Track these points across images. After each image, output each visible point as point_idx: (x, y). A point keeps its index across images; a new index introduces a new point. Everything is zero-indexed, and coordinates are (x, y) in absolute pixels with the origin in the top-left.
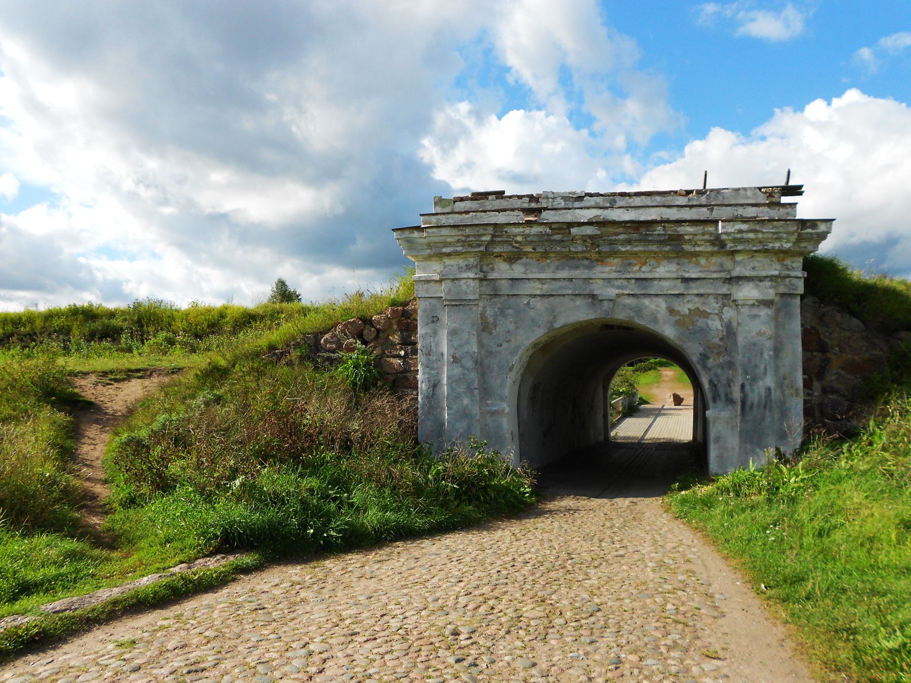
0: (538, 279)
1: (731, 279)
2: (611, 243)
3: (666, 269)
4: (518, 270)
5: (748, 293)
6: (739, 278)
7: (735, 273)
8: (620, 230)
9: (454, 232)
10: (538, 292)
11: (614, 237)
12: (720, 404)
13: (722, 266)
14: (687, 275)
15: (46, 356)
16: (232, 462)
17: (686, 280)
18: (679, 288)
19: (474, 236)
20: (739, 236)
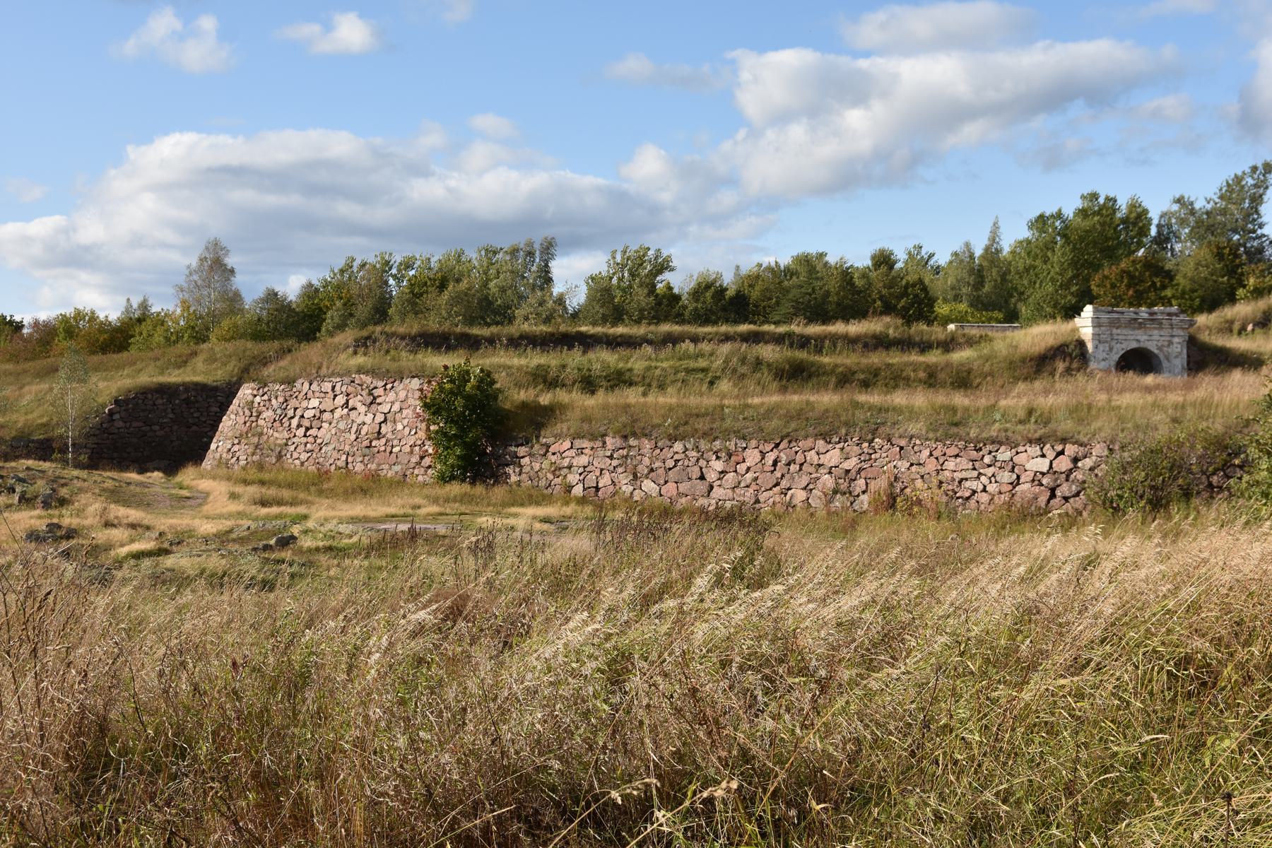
3: (1156, 332)
5: (1176, 340)
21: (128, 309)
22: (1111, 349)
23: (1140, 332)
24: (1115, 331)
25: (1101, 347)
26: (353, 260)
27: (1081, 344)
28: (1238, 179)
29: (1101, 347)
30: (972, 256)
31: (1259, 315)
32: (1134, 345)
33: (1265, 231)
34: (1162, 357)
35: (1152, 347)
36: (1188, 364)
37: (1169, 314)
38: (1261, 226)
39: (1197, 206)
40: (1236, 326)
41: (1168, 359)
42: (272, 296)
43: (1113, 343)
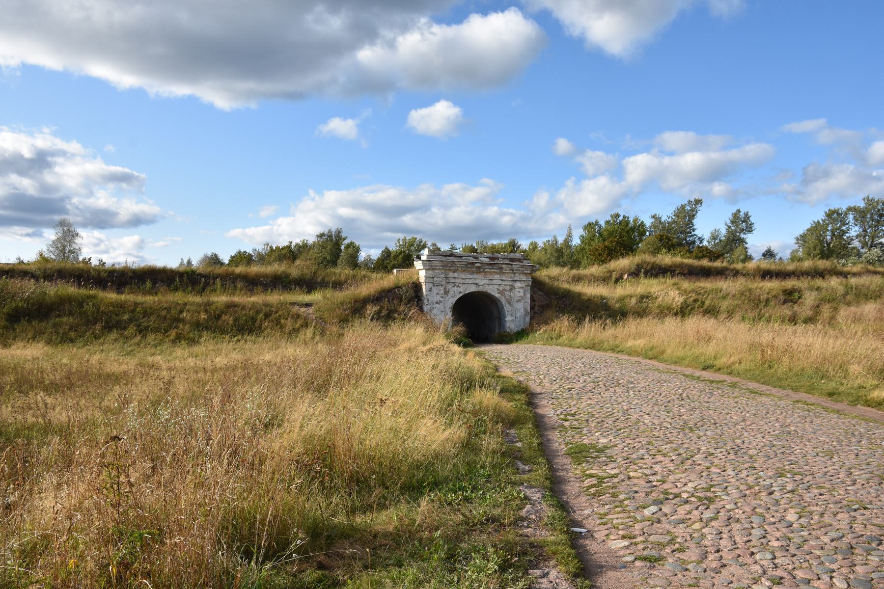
3: (497, 277)
4: (456, 275)
5: (518, 284)
18: (500, 282)
21: (182, 264)
22: (446, 292)
23: (479, 276)
24: (451, 275)
25: (435, 290)
27: (417, 286)
28: (683, 207)
29: (435, 290)
30: (557, 242)
31: (633, 268)
32: (473, 289)
33: (696, 232)
34: (503, 301)
35: (493, 291)
36: (532, 308)
37: (512, 260)
38: (694, 230)
39: (663, 220)
40: (614, 276)
41: (510, 303)
43: (449, 286)
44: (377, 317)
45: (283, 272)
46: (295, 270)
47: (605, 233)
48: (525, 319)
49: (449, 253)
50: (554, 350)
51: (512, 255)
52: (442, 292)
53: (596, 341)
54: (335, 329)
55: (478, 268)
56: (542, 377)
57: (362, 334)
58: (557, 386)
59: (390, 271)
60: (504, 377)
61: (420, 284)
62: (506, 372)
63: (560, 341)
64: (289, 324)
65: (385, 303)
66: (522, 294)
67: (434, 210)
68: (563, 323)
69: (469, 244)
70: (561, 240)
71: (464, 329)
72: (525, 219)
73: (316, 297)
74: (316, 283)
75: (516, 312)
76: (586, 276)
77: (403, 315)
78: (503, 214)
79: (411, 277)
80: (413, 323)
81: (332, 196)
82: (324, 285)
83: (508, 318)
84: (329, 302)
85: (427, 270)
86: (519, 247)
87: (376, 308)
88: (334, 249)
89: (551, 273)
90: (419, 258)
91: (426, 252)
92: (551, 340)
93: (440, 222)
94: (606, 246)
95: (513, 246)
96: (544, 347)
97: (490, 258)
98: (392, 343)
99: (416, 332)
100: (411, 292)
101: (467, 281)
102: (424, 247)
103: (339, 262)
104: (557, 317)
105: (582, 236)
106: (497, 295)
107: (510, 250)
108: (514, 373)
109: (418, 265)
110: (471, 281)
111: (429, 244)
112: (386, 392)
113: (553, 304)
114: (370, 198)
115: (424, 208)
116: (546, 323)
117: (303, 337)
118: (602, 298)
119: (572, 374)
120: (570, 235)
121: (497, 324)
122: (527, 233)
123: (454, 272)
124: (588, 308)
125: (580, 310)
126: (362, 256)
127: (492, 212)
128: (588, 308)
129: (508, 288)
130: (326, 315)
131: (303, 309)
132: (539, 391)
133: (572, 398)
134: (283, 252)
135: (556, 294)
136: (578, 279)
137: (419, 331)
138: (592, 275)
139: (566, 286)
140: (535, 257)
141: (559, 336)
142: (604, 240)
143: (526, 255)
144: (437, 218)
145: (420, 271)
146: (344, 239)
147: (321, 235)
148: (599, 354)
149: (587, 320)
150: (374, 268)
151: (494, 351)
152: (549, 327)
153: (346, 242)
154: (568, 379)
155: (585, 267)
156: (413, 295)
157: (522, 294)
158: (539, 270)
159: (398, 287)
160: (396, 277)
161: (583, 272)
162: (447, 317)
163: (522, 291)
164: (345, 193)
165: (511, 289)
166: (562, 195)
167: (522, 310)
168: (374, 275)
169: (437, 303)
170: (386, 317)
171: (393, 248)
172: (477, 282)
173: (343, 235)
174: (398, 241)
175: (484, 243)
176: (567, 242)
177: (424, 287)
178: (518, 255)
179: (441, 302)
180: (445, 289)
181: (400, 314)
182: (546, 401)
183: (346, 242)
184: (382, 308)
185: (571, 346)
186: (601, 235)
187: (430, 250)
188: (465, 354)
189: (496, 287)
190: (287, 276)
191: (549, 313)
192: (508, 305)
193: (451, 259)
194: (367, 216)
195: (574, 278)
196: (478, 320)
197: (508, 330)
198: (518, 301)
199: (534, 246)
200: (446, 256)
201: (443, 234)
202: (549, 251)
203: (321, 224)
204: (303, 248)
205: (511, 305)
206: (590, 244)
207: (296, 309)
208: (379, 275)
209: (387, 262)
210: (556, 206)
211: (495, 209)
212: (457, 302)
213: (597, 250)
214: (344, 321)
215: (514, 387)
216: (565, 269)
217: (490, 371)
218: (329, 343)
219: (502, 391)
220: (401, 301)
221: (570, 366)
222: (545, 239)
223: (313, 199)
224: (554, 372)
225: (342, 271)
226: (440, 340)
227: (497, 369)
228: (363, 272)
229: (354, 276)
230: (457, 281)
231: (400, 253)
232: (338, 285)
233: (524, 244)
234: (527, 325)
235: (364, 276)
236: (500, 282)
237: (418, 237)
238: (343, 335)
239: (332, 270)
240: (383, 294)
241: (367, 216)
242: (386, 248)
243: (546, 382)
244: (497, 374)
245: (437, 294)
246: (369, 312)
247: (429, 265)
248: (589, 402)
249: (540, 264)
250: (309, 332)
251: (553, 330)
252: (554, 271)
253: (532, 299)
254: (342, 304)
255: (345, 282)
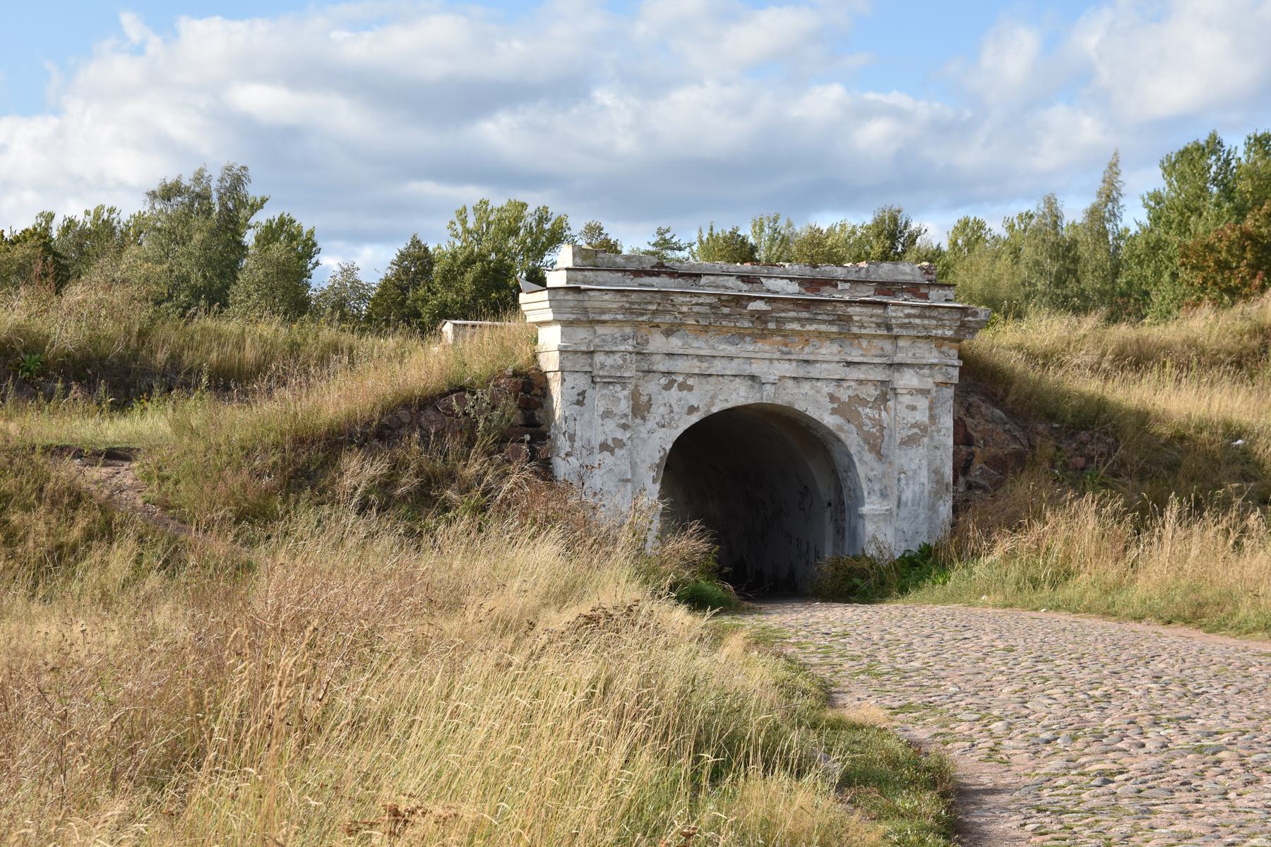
0: (697, 356)
1: (891, 365)
2: (779, 321)
3: (828, 350)
4: (675, 343)
5: (907, 380)
6: (901, 365)
7: (897, 360)
8: (790, 307)
9: (618, 297)
10: (697, 371)
11: (783, 315)
12: (873, 498)
13: (882, 349)
14: (849, 359)
15: (1121, 226)
16: (113, 639)
17: (849, 364)
18: (840, 372)
19: (639, 304)
20: (906, 321)
22: (640, 409)
23: (764, 348)
24: (658, 342)
26: (51, 217)
27: (530, 387)
29: (598, 400)
30: (1056, 218)
32: (739, 396)
34: (852, 440)
36: (962, 467)
37: (887, 287)
41: (876, 447)
42: (348, 272)
43: (652, 387)
44: (380, 499)
45: (18, 330)
46: (68, 319)
47: (1244, 186)
48: (933, 508)
49: (649, 263)
50: (1042, 626)
51: (886, 271)
52: (624, 406)
53: (1208, 594)
54: (220, 547)
55: (760, 317)
56: (997, 727)
57: (329, 563)
58: (1056, 764)
59: (426, 329)
60: (856, 727)
61: (543, 375)
62: (862, 706)
63: (1069, 592)
64: (38, 527)
65: (412, 448)
66: (922, 416)
67: (604, 96)
68: (1081, 526)
69: (723, 228)
70: (1074, 211)
71: (703, 546)
72: (943, 130)
73: (149, 423)
74: (148, 372)
75: (897, 492)
76: (1167, 348)
77: (476, 494)
78: (866, 113)
79: (507, 353)
80: (514, 520)
81: (208, 40)
82: (176, 379)
83: (871, 506)
84: (200, 446)
85: (566, 324)
86: (912, 239)
87: (377, 468)
88: (219, 247)
89: (1034, 338)
90: (537, 279)
91: (564, 256)
92: (1046, 583)
93: (625, 144)
94: (1246, 235)
95: (892, 237)
96: (1007, 616)
97: (802, 281)
98: (440, 597)
99: (535, 559)
100: (510, 409)
101: (718, 367)
102: (556, 238)
103: (236, 293)
104: (1055, 502)
105: (1157, 198)
106: (830, 420)
107: (878, 250)
108: (894, 711)
109: (534, 304)
110: (732, 368)
111: (576, 226)
112: (411, 784)
113: (1032, 450)
114: (357, 49)
115: (567, 88)
116: (1014, 525)
117: (93, 575)
118: (1232, 431)
119: (1115, 718)
120: (1110, 194)
121: (829, 530)
122: (953, 186)
123: (668, 333)
124: (1173, 467)
125: (1142, 475)
126: (327, 269)
127: (822, 102)
128: (1173, 467)
129: (871, 392)
130: (186, 493)
131: (99, 472)
132: (987, 781)
133: (1115, 808)
134: (18, 253)
135: (1051, 417)
136: (1138, 360)
137: (542, 556)
138: (1191, 344)
139: (1092, 386)
140: (973, 276)
141: (1064, 575)
142: (1241, 212)
143: (938, 269)
144: (614, 126)
145: (541, 329)
146: (256, 207)
147: (169, 192)
148: (1220, 644)
149: (1171, 513)
150: (369, 319)
151: (812, 626)
152: (1025, 541)
153: (261, 218)
154: (1100, 737)
155: (1166, 315)
156: (517, 418)
157: (922, 416)
158: (985, 324)
159: (459, 389)
160: (451, 351)
161: (1154, 331)
162: (644, 501)
163: (923, 403)
164: (261, 26)
165: (883, 399)
166: (1090, 38)
167: (924, 476)
168: (369, 342)
169: (604, 447)
170: (416, 503)
171: (441, 240)
172: (755, 369)
173: (252, 191)
174: (462, 215)
175: (782, 224)
176: (1099, 217)
177: (556, 389)
178: (908, 271)
179: (620, 443)
180: (635, 396)
181: (465, 490)
182: (1017, 819)
183: (261, 218)
184: (397, 467)
185: (1108, 613)
186: (1228, 193)
187: (578, 252)
188: (717, 639)
189: (826, 389)
190: (36, 345)
191: (1023, 487)
192: (869, 457)
193: (659, 283)
194: (345, 118)
195: (1120, 355)
196: (756, 510)
197: (871, 551)
198: (910, 441)
199: (971, 234)
200: (638, 273)
201: (628, 191)
202: (1027, 252)
203: (164, 144)
204: (98, 238)
205: (880, 456)
206: (1183, 228)
207: (69, 469)
208: (391, 342)
209: (414, 296)
210: (1072, 83)
211: (835, 92)
212: (680, 443)
213: (1210, 248)
214: (254, 516)
215: (894, 763)
216: (1090, 323)
217: (800, 703)
218: (200, 599)
219: (846, 781)
220: (470, 443)
221: (1108, 687)
222: (1015, 209)
223: (139, 50)
224: (1046, 707)
225: (249, 329)
226: (615, 586)
227: (828, 696)
228: (328, 334)
229: (294, 348)
230: (680, 365)
231: (469, 262)
232: (229, 381)
233: (934, 229)
234: (942, 531)
235: (335, 348)
236: (840, 372)
237: (534, 201)
238: (249, 567)
239: (210, 323)
240: (405, 415)
241: (345, 118)
242: (416, 243)
243: (1013, 746)
244: (830, 714)
245: (607, 414)
246: (348, 482)
247: (575, 307)
248: (1182, 826)
249: (993, 303)
250: (119, 558)
251: (1040, 549)
252: (1046, 329)
253: (963, 437)
254: (249, 452)
255: (260, 368)
